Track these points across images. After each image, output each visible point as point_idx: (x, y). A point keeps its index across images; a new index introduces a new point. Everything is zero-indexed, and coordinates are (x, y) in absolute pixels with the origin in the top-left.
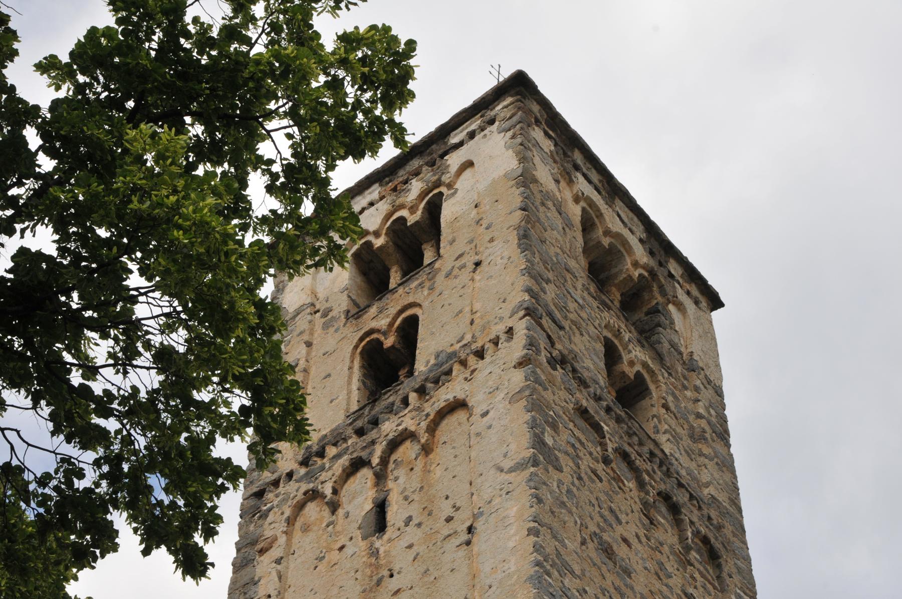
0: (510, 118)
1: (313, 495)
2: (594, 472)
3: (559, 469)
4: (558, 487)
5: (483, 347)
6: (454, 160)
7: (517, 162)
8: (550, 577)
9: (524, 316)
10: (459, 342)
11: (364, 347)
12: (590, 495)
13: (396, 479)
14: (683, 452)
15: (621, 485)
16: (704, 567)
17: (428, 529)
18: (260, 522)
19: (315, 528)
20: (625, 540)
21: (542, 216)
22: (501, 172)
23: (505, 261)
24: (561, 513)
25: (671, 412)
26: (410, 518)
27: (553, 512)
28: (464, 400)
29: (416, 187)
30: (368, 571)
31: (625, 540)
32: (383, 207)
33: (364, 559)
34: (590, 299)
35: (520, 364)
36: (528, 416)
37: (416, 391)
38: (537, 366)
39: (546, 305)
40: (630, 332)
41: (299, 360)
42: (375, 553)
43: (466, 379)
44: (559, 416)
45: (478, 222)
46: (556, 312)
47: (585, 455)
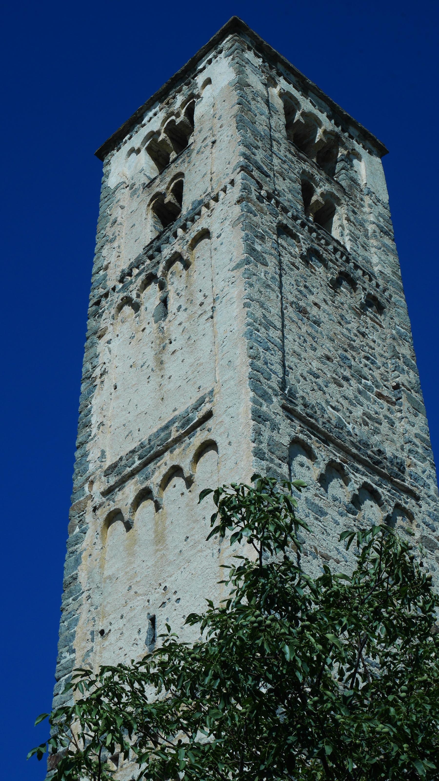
0: (231, 47)
1: (127, 301)
2: (293, 264)
3: (266, 265)
4: (265, 276)
5: (217, 194)
6: (200, 79)
7: (235, 75)
8: (258, 331)
9: (240, 171)
10: (205, 193)
11: (153, 204)
12: (290, 279)
13: (173, 283)
14: (360, 246)
15: (313, 270)
16: (374, 315)
17: (190, 312)
18: (99, 320)
19: (129, 320)
20: (316, 304)
21: (253, 107)
22: (226, 82)
23: (229, 138)
24: (267, 292)
25: (351, 222)
26: (180, 307)
27: (261, 292)
28: (207, 229)
29: (180, 99)
30: (158, 342)
31: (316, 304)
32: (162, 115)
33: (156, 335)
34: (290, 156)
35: (239, 202)
36: (243, 234)
37: (181, 227)
38: (248, 202)
39: (256, 162)
40: (321, 174)
41: (117, 218)
42: (161, 330)
43: (208, 216)
44: (266, 232)
45: (213, 116)
46: (264, 167)
47: (286, 254)
